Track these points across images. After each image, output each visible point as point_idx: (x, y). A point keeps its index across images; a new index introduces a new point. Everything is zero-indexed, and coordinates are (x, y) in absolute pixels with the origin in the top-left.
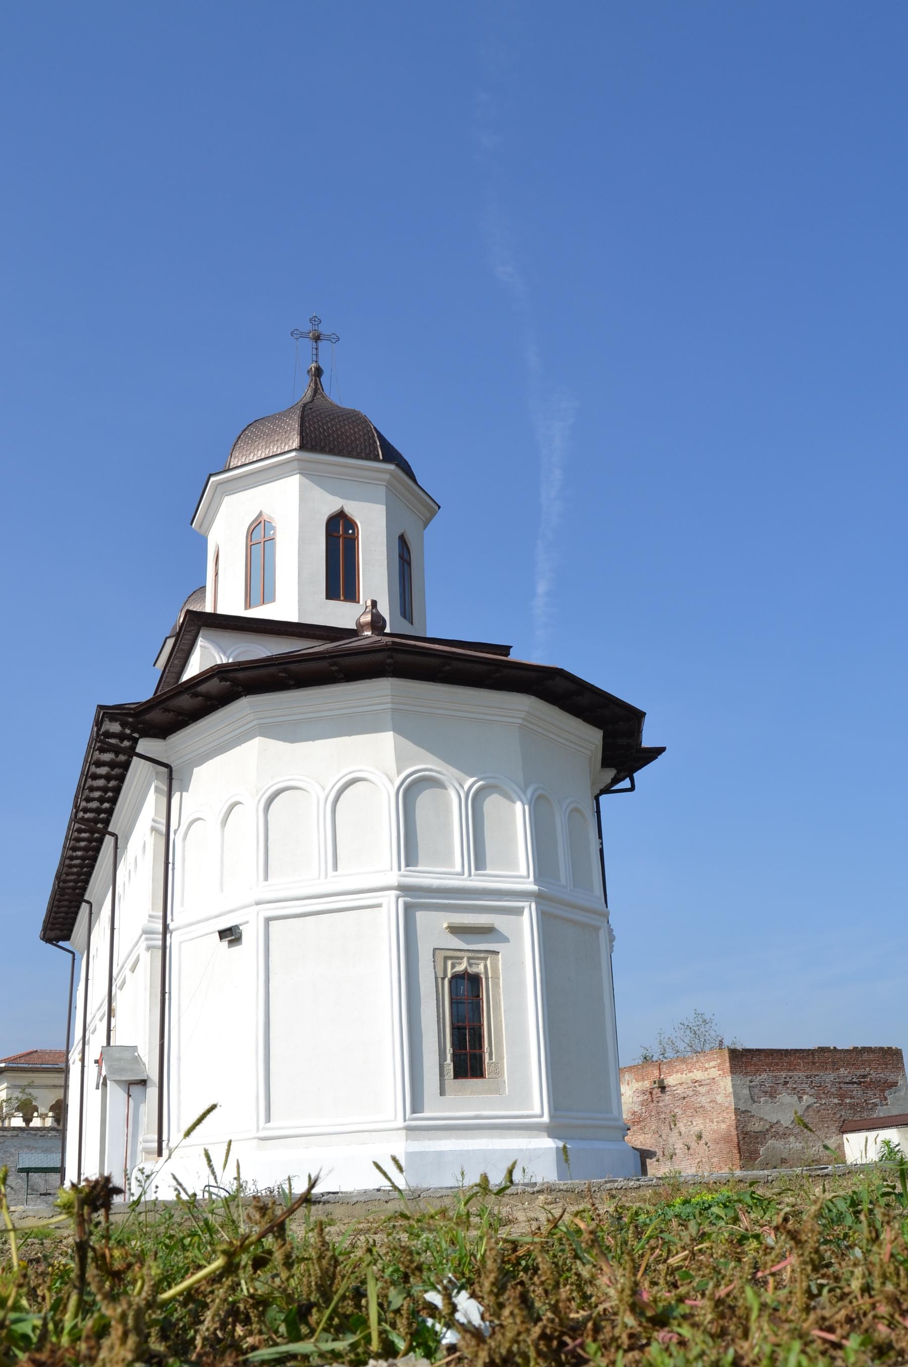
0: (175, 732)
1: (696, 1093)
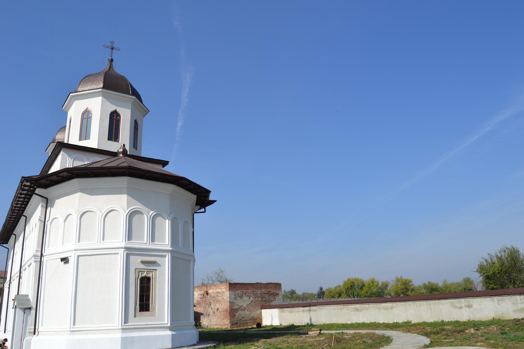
1: (218, 296)
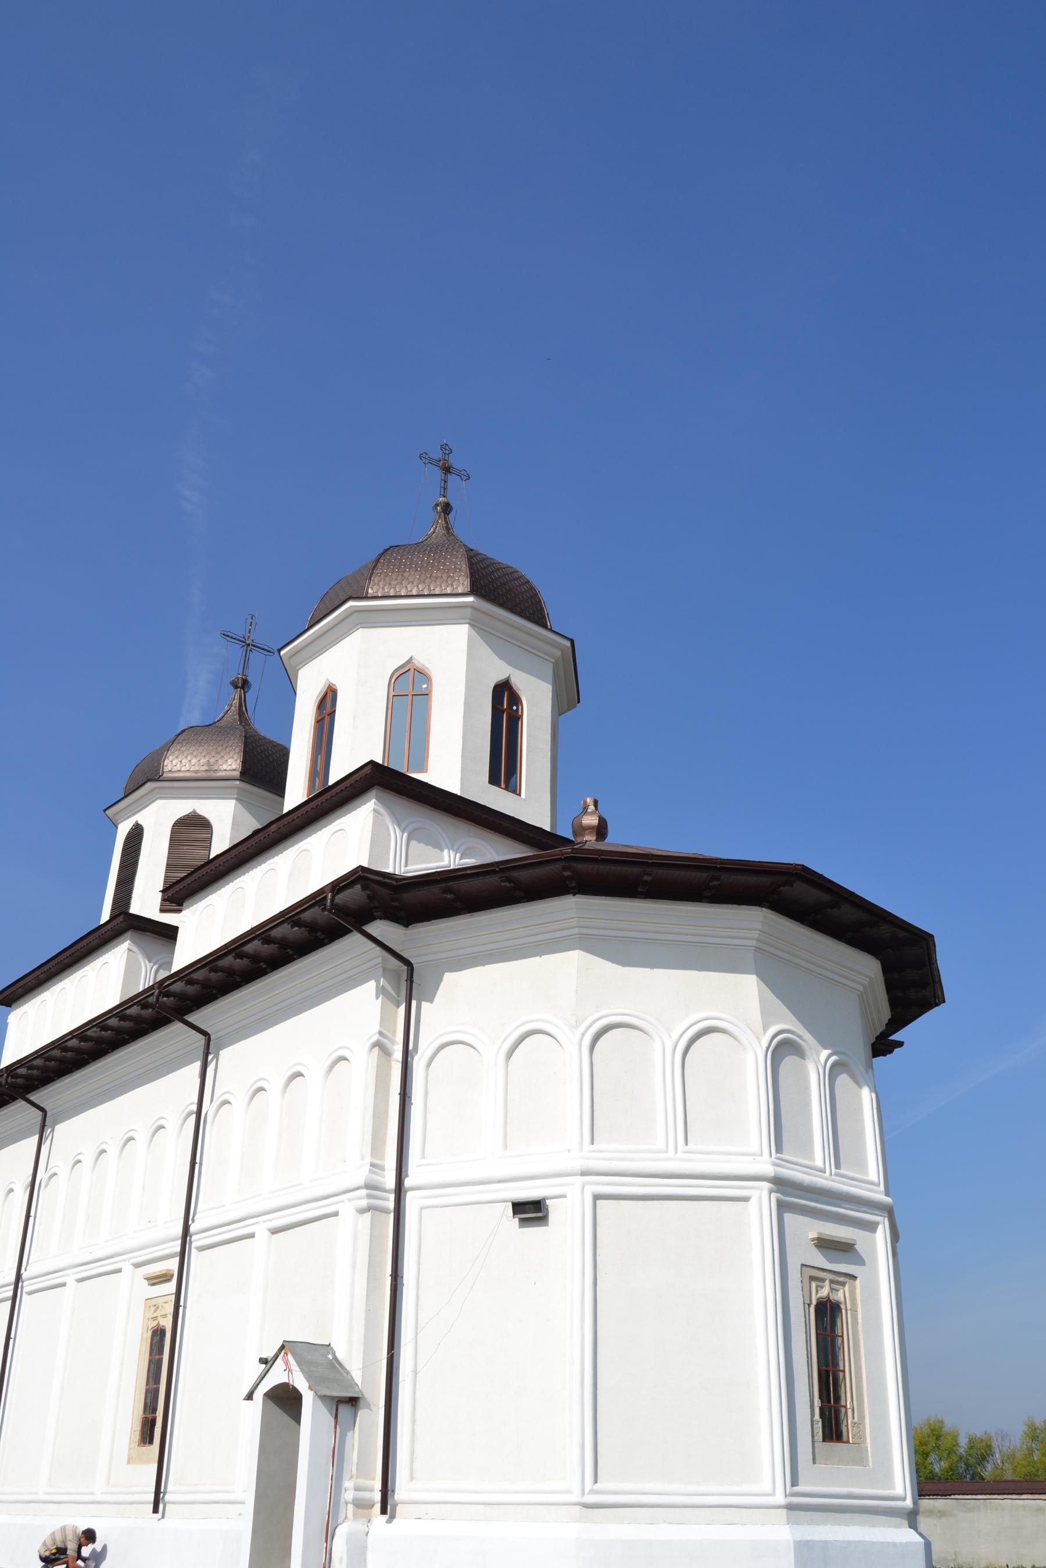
0: (423, 921)
